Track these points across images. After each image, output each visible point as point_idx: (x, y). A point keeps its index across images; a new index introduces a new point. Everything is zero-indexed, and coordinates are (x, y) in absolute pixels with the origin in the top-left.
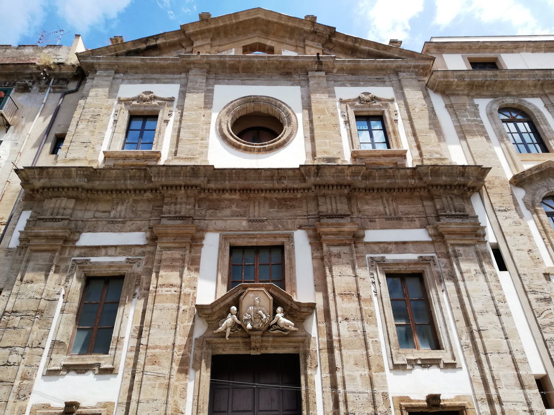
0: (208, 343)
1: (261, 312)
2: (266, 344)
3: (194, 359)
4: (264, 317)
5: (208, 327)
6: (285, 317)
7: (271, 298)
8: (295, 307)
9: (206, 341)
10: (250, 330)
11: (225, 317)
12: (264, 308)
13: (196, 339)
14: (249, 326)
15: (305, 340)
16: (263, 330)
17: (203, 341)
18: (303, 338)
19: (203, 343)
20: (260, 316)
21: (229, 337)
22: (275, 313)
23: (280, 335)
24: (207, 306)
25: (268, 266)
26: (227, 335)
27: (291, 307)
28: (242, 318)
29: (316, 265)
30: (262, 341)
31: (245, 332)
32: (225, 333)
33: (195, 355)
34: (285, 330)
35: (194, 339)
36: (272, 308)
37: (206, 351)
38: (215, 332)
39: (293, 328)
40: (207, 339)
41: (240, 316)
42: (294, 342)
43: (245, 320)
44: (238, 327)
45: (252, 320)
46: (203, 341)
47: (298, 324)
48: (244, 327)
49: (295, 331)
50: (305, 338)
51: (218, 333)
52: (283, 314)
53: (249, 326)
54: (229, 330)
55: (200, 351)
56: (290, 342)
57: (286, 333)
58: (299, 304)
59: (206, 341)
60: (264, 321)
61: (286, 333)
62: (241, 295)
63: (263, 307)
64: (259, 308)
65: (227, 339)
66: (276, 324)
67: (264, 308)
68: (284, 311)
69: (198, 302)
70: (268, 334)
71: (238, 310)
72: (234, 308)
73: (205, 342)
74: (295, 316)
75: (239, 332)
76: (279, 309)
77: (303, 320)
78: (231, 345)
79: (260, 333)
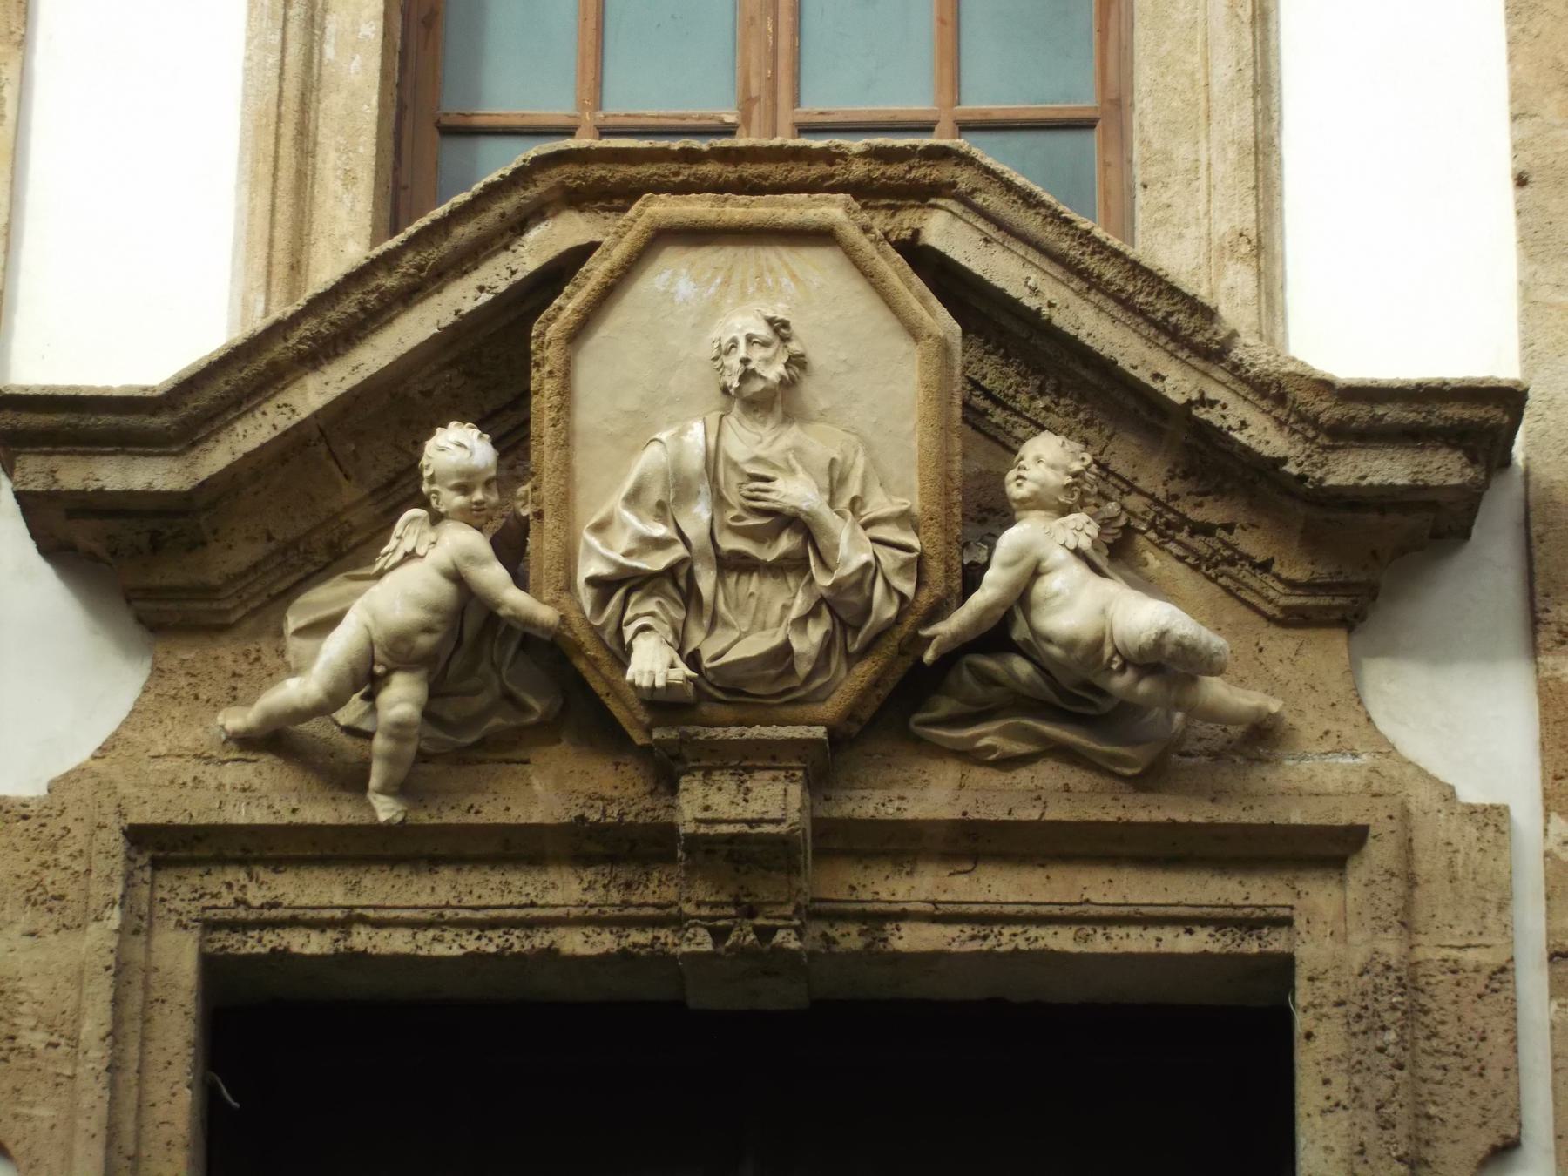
7: (942, 322)
14: (652, 662)
22: (988, 511)
41: (542, 546)
52: (1080, 528)
53: (652, 662)
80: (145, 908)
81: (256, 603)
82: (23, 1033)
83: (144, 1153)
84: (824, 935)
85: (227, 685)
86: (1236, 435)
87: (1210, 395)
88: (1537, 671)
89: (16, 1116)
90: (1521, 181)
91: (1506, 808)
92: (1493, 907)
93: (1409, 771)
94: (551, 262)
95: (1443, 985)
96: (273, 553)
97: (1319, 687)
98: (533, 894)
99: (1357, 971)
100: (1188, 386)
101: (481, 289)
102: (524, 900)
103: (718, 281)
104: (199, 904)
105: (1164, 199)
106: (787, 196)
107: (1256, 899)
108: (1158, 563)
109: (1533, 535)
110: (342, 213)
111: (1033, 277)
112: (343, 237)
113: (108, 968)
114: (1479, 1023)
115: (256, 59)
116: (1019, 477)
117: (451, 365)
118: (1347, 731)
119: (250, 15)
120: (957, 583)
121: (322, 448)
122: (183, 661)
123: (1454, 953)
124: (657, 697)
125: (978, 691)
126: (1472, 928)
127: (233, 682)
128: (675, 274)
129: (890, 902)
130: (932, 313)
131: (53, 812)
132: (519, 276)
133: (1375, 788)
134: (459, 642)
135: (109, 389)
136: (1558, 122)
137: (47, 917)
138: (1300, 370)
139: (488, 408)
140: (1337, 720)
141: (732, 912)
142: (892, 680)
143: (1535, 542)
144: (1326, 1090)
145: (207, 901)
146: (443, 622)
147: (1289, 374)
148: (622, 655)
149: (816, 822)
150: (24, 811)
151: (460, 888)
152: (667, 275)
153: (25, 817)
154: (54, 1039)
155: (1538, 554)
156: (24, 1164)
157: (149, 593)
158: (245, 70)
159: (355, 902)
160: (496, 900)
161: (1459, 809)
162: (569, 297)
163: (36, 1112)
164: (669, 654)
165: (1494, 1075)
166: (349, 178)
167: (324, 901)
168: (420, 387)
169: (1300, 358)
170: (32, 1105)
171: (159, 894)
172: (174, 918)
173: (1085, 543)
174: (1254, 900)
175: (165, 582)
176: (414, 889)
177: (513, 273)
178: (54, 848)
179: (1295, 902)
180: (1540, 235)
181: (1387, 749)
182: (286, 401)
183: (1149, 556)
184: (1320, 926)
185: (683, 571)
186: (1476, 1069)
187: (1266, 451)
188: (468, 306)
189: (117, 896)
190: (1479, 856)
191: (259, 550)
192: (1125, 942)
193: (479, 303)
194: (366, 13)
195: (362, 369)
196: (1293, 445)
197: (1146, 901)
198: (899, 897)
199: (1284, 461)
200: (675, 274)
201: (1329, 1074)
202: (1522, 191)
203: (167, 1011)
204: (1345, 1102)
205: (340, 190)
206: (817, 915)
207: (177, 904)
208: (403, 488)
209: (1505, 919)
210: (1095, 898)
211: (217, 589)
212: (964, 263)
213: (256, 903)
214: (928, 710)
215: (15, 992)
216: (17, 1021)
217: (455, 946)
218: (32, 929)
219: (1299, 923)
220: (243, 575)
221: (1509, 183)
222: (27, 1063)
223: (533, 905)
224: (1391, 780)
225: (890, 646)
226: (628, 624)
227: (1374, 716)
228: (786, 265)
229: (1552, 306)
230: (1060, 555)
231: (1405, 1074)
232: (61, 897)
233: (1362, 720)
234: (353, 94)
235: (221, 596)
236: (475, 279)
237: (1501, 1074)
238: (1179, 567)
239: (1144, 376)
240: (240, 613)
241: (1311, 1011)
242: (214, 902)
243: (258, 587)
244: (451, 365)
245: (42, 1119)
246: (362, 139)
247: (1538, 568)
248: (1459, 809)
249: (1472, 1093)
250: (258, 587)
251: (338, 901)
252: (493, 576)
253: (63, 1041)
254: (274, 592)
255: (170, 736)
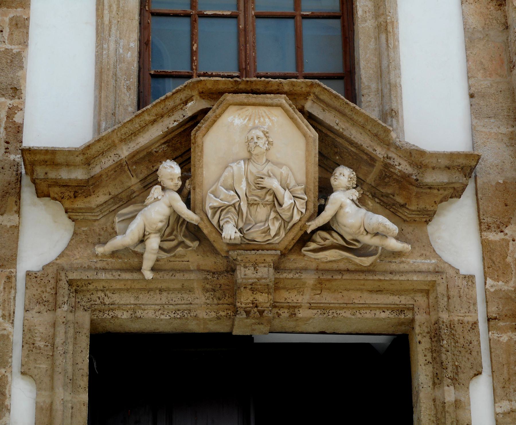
0: (76, 287)
1: (274, 184)
2: (293, 297)
3: (25, 343)
4: (287, 201)
5: (75, 234)
6: (360, 202)
7: (314, 134)
8: (403, 166)
9: (70, 283)
10: (233, 246)
11: (137, 198)
12: (284, 170)
13: (28, 274)
14: (230, 232)
15: (433, 284)
16: (282, 247)
17: (58, 281)
18: (430, 278)
19: (56, 288)
20: (269, 198)
21: (153, 269)
22: (325, 190)
23: (342, 266)
24: (70, 152)
25: (291, 22)
26: (148, 263)
27: (387, 166)
28: (203, 202)
29: (475, 22)
30: (277, 286)
31: (215, 251)
32: (140, 256)
33: (28, 331)
34: (363, 251)
35: (21, 275)
36: (315, 170)
37: (70, 317)
38: (100, 250)
39: (394, 244)
40: (73, 276)
41: (196, 197)
42: (393, 293)
43: (215, 210)
44: (182, 231)
45: (239, 212)
46: (58, 281)
47: (408, 229)
48: (212, 236)
49: (397, 254)
50: (437, 278)
51: (114, 254)
52: (355, 194)
53: (230, 232)
54: (154, 242)
55: (48, 317)
56: (379, 291)
57: (366, 261)
58: (418, 157)
59: (70, 283)
60: (286, 216)
61: (366, 261)
62: (196, 119)
63: (279, 165)
64: (269, 167)
65: (149, 275)
66: (327, 228)
67: (284, 170)
68: (360, 183)
69: (31, 139)
70: (301, 263)
71: (184, 178)
72: (170, 170)
73: (64, 284)
74: (400, 200)
75: (192, 256)
76: (343, 176)
77: (428, 216)
78: (164, 298)
79: (270, 256)
80: (73, 304)
81: (105, 214)
82: (37, 342)
83: (75, 378)
84: (277, 313)
85: (97, 238)
86: (397, 167)
87: (390, 155)
88: (481, 237)
89: (35, 368)
90: (472, 96)
91: (474, 276)
92: (472, 304)
93: (446, 265)
94: (195, 113)
95: (459, 328)
96: (112, 198)
97: (419, 241)
98: (191, 300)
99: (433, 323)
100: (383, 153)
101: (175, 121)
102: (188, 302)
103: (247, 119)
104: (90, 303)
105: (369, 99)
106: (268, 95)
107: (403, 302)
108: (372, 205)
109: (479, 198)
110: (126, 98)
111: (337, 120)
112: (127, 106)
113: (63, 323)
114: (469, 339)
115: (99, 52)
116: (335, 178)
117: (164, 143)
118: (428, 254)
119: (97, 39)
120: (317, 209)
121: (127, 167)
122: (83, 231)
123: (461, 318)
124: (232, 242)
125: (323, 242)
126: (466, 311)
127: (99, 237)
128: (234, 117)
129: (296, 303)
130: (310, 130)
131: (45, 276)
132: (185, 118)
133: (437, 270)
134: (168, 226)
135: (64, 148)
136: (482, 79)
137: (44, 307)
138: (416, 148)
139: (174, 157)
140: (425, 250)
141: (251, 305)
142: (298, 238)
143: (480, 200)
144: (425, 358)
145: (92, 302)
146: (166, 219)
147: (413, 149)
148: (219, 229)
149: (276, 278)
150: (36, 275)
151: (169, 299)
152: (232, 117)
153: (36, 277)
154: (47, 344)
155: (480, 203)
156: (38, 382)
157: (74, 210)
158: (96, 55)
159: (137, 302)
160: (180, 302)
161: (461, 276)
162: (203, 124)
163: (41, 366)
164: (236, 230)
165: (474, 353)
166: (129, 88)
167: (128, 302)
168: (155, 150)
169: (416, 145)
170: (40, 364)
171: (77, 300)
172: (82, 308)
173: (355, 198)
174: (403, 302)
175: (79, 206)
176: (155, 299)
177: (184, 116)
178: (45, 286)
179: (414, 303)
180: (478, 111)
181: (439, 257)
182: (117, 153)
183: (369, 203)
184: (422, 310)
185: (237, 205)
186: (469, 352)
187: (407, 172)
188: (171, 126)
189: (66, 301)
190: (467, 290)
191: (107, 197)
192: (365, 314)
193: (174, 125)
194: (132, 40)
195: (140, 144)
196: (414, 170)
197: (371, 303)
198: (299, 301)
199: (412, 175)
200: (234, 117)
201: (426, 353)
202: (472, 99)
203: (81, 335)
204: (431, 361)
205: (126, 92)
206: (275, 307)
207: (83, 303)
208: (151, 180)
209: (475, 308)
210: (356, 301)
211: (94, 209)
212: (317, 116)
213: (107, 303)
214: (307, 246)
215: (34, 330)
216: (35, 339)
217: (168, 316)
218: (39, 311)
219: (416, 309)
220: (102, 205)
221: (467, 97)
222: (38, 351)
223: (191, 304)
224: (441, 268)
225: (297, 229)
226: (221, 220)
227: (435, 249)
228: (267, 115)
229: (482, 132)
230: (349, 202)
231: (449, 353)
232: (48, 301)
233: (432, 250)
234: (128, 63)
235: (95, 211)
236: (173, 118)
237: (476, 353)
238: (378, 205)
239: (370, 149)
240: (101, 216)
241: (420, 335)
242: (94, 303)
243: (106, 209)
244: (164, 143)
245: (43, 368)
246: (132, 77)
247: (481, 207)
248: (461, 276)
249: (468, 359)
250: (106, 209)
251: (132, 302)
252: (181, 206)
253: (49, 345)
254: (111, 210)
255: (80, 253)
